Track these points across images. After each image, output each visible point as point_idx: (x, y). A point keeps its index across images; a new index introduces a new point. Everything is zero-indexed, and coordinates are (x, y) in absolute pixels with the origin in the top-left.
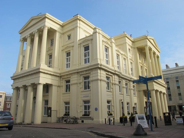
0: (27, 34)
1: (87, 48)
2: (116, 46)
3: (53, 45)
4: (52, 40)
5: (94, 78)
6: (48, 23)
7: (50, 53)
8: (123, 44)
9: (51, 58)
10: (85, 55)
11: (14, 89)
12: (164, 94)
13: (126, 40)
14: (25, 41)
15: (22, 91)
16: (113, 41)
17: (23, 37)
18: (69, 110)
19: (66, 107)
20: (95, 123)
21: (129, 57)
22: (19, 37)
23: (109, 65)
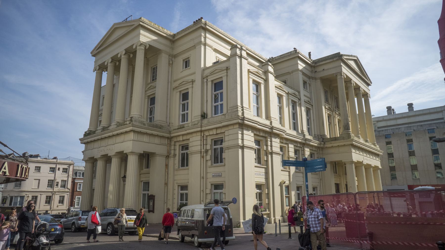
0: (107, 57)
1: (218, 86)
2: (277, 77)
3: (156, 79)
4: (154, 69)
5: (231, 143)
6: (145, 36)
7: (153, 93)
8: (292, 72)
9: (154, 104)
10: (215, 99)
11: (86, 161)
12: (376, 168)
13: (298, 64)
14: (103, 71)
15: (100, 165)
16: (271, 69)
17: (100, 62)
18: (187, 200)
19: (182, 195)
20: (422, 198)
21: (303, 98)
22: (91, 62)
23: (262, 117)
